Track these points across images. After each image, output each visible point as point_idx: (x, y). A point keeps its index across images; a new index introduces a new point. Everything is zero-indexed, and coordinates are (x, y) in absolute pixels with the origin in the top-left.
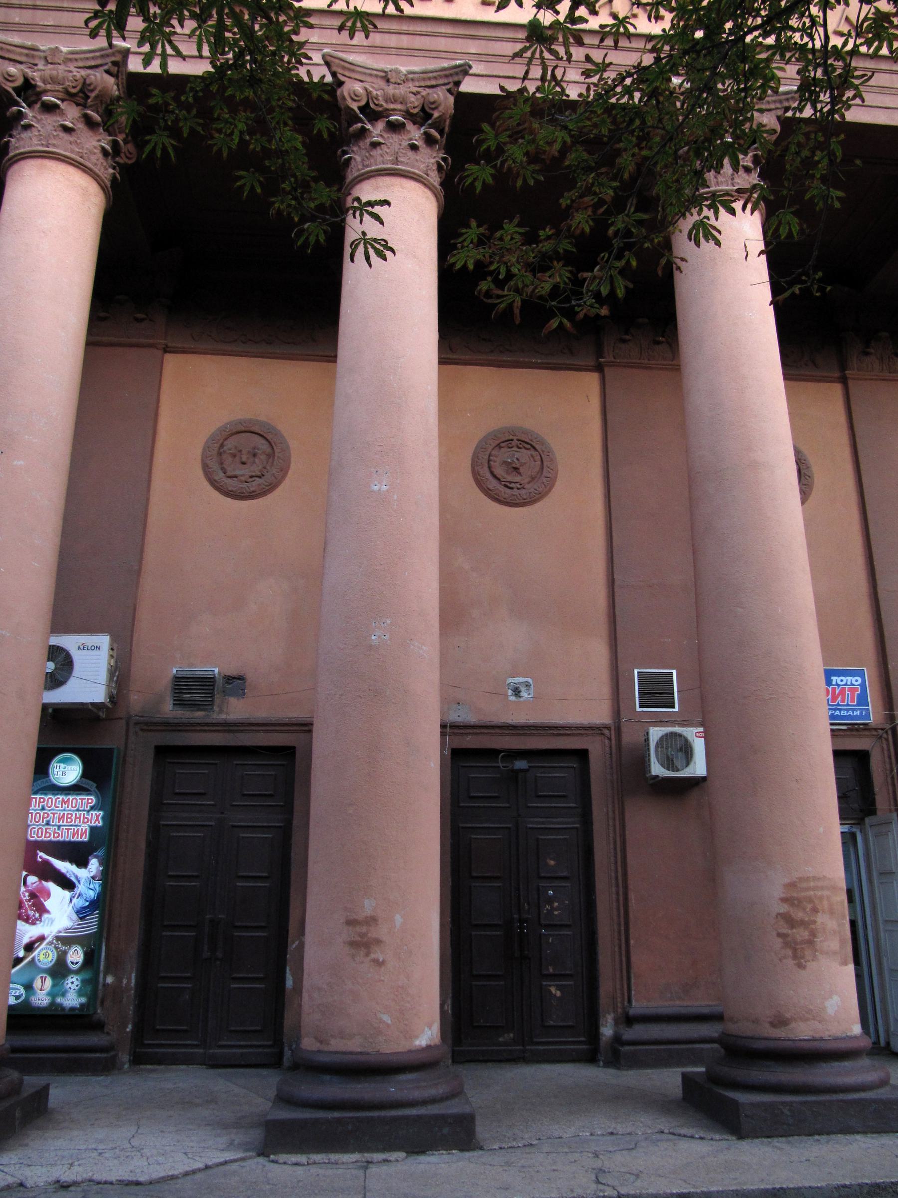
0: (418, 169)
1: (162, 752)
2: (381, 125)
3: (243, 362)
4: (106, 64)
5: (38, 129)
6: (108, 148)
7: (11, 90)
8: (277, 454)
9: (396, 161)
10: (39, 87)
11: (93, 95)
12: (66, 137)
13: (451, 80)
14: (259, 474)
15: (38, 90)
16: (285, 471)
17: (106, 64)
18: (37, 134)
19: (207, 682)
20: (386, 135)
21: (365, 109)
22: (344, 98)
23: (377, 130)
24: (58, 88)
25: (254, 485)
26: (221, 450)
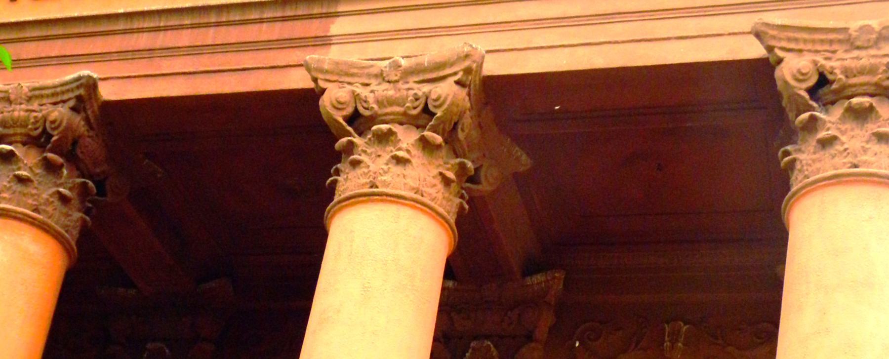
2: (837, 111)
4: (455, 74)
5: (367, 164)
6: (451, 175)
7: (341, 120)
13: (71, 95)
17: (455, 74)
21: (354, 118)
22: (786, 82)
23: (831, 119)
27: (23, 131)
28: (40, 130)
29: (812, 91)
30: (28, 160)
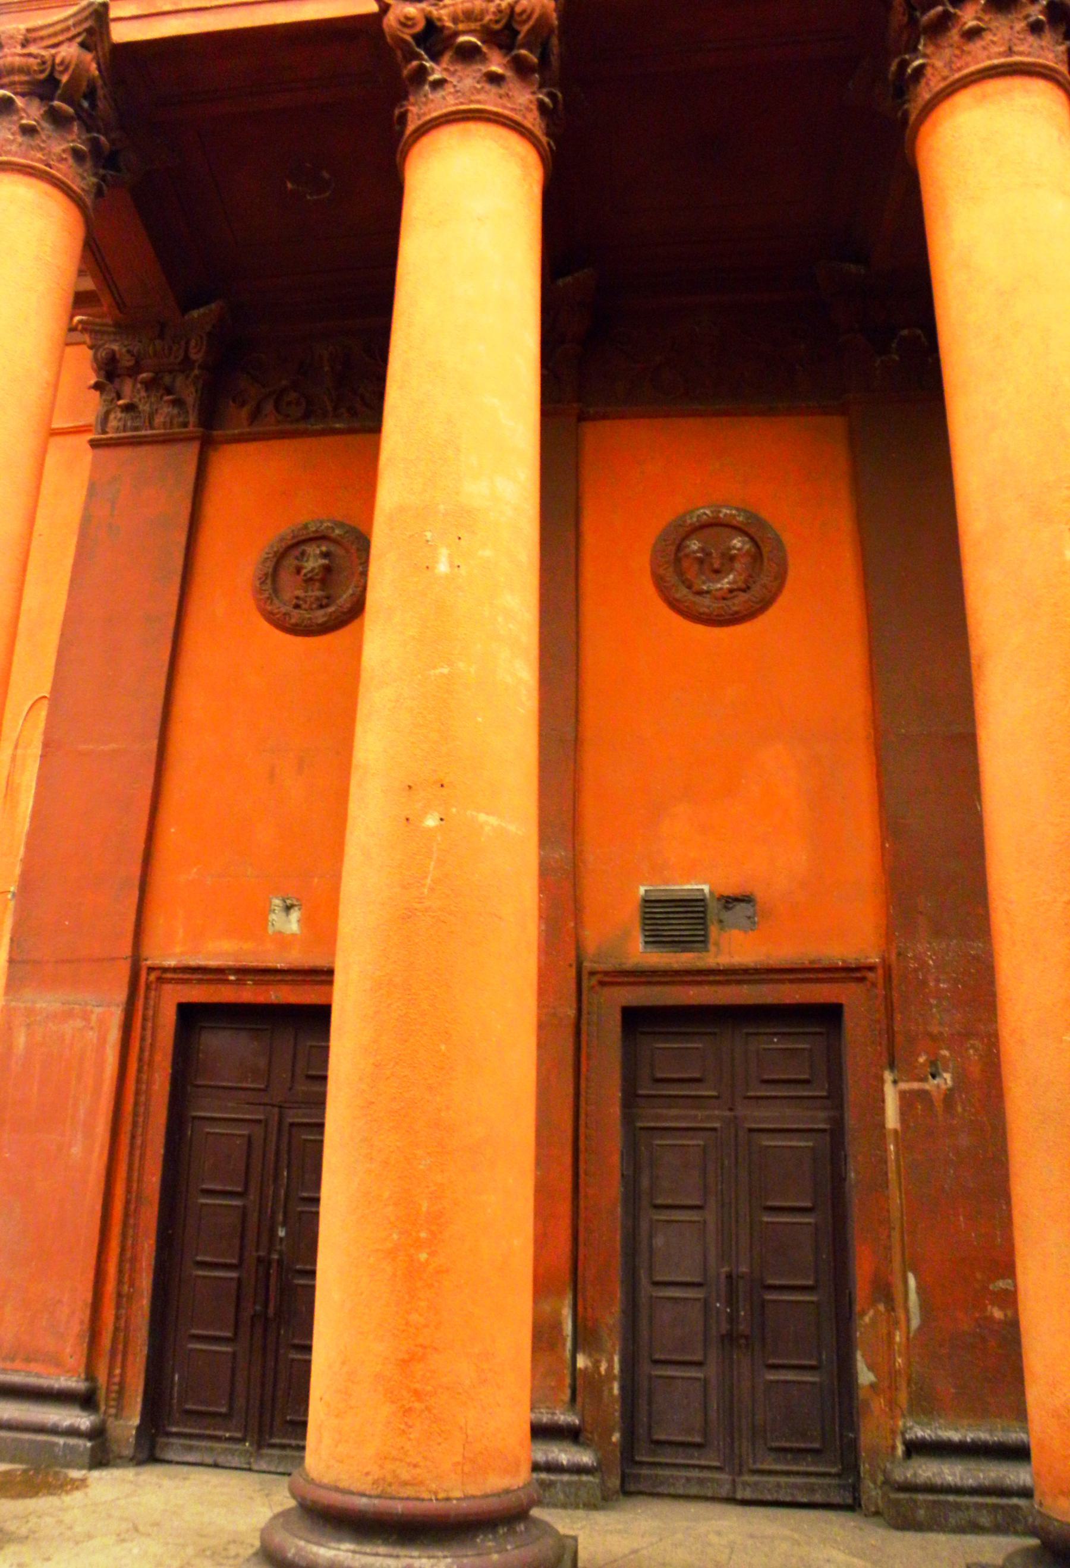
0: (1047, 59)
1: (634, 1019)
3: (695, 424)
8: (765, 555)
9: (1010, 52)
10: (448, 28)
11: (525, 28)
12: (493, 89)
13: (79, 29)
14: (744, 586)
15: (446, 32)
16: (781, 577)
18: (452, 90)
19: (692, 910)
20: (986, 18)
24: (473, 26)
25: (738, 603)
26: (681, 554)
27: (24, 78)
28: (46, 73)
29: (417, 37)
30: (31, 112)
